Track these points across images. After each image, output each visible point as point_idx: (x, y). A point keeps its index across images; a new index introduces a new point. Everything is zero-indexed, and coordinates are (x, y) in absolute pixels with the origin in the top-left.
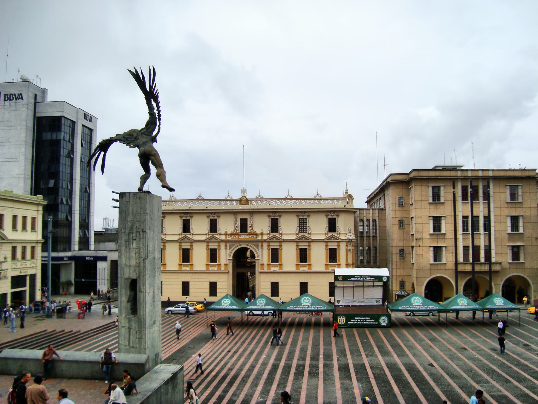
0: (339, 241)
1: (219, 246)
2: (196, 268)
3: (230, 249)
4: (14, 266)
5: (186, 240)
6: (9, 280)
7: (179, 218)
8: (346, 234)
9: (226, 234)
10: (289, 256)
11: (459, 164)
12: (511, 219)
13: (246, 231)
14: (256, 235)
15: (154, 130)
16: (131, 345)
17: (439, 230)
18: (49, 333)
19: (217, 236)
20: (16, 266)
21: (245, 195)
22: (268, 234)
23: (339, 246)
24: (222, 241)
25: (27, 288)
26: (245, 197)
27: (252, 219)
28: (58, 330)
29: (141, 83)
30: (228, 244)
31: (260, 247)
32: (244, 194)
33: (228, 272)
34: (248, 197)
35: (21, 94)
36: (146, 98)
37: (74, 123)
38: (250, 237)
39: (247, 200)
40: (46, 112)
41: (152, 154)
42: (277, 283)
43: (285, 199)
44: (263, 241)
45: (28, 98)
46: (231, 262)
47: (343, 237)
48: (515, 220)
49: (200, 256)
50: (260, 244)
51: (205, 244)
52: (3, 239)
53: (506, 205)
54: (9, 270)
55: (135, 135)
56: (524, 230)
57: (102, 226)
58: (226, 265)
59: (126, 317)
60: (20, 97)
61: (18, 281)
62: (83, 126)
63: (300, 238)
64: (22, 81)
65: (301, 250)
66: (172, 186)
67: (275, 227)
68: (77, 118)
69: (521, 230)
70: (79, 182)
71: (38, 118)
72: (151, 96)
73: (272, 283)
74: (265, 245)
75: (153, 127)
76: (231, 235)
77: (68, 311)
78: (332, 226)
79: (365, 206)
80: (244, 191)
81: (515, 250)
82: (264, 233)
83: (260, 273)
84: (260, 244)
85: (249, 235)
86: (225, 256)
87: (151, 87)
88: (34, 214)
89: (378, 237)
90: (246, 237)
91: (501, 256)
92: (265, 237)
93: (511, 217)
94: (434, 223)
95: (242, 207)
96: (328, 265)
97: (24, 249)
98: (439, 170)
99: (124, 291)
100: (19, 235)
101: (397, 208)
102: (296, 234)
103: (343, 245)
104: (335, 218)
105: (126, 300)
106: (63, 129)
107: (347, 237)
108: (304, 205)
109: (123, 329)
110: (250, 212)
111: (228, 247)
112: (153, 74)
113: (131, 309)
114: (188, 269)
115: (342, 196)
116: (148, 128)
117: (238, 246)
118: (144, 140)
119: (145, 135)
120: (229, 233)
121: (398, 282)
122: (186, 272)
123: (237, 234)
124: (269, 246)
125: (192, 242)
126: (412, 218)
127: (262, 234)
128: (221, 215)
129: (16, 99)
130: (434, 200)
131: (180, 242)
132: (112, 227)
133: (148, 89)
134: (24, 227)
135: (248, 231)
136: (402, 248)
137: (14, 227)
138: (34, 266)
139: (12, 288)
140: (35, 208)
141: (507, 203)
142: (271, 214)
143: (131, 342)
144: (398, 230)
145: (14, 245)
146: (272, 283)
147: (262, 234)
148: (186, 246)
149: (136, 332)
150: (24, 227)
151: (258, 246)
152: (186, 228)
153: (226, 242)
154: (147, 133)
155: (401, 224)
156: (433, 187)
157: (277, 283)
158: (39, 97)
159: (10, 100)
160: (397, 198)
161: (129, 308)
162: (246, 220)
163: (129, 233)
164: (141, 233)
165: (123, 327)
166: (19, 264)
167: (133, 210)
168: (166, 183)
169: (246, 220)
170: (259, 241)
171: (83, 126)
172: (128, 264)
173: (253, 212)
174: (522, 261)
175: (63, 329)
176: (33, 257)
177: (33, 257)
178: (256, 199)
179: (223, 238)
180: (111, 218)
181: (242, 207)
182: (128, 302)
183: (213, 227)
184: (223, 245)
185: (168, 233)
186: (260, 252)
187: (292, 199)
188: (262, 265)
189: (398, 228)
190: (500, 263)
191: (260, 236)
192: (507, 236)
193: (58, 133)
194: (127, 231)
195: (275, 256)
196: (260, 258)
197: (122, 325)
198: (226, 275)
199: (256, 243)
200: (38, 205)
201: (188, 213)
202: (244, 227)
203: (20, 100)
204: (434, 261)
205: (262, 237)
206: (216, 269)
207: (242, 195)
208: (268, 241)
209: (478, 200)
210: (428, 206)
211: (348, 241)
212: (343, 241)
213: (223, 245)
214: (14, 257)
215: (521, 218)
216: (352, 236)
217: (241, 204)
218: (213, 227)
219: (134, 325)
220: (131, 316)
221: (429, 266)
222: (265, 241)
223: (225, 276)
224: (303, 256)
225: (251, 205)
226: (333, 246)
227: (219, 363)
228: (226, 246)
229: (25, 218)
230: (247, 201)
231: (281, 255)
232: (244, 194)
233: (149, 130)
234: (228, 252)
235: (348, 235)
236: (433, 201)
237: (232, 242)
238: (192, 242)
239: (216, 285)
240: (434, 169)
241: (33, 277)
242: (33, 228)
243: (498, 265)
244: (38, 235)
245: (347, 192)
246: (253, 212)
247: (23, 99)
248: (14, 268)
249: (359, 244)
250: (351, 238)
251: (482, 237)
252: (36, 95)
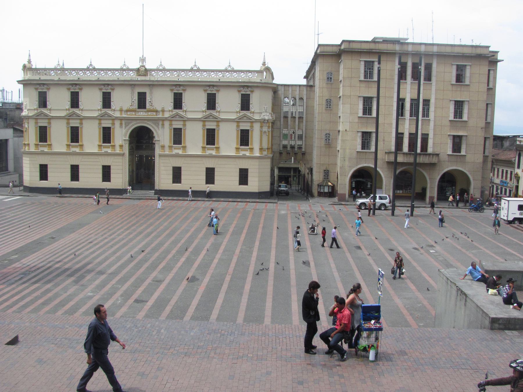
0: (252, 122)
1: (113, 124)
5: (211, 119)
7: (34, 90)
8: (261, 113)
9: (121, 110)
10: (194, 137)
11: (401, 36)
12: (455, 104)
13: (145, 107)
14: (157, 111)
17: (461, 117)
21: (145, 64)
22: (170, 111)
23: (252, 127)
24: (117, 118)
26: (144, 66)
27: (151, 93)
30: (123, 122)
31: (160, 126)
32: (143, 63)
33: (123, 155)
38: (149, 113)
39: (146, 70)
43: (191, 70)
44: (163, 120)
46: (127, 142)
47: (257, 117)
48: (459, 105)
50: (161, 123)
53: (450, 87)
56: (468, 118)
58: (121, 146)
63: (240, 118)
65: (242, 131)
67: (178, 103)
69: (465, 118)
74: (167, 124)
76: (127, 111)
77: (504, 310)
78: (245, 104)
79: (304, 82)
80: (143, 60)
81: (457, 140)
83: (160, 156)
84: (161, 123)
86: (121, 136)
89: (304, 119)
90: (144, 114)
91: (439, 144)
92: (167, 115)
93: (456, 101)
94: (364, 105)
95: (140, 78)
98: (378, 42)
101: (324, 84)
103: (257, 127)
107: (262, 117)
108: (214, 77)
110: (149, 85)
111: (124, 125)
115: (258, 69)
120: (125, 109)
121: (322, 171)
124: (171, 125)
126: (340, 97)
127: (163, 111)
128: (83, 87)
130: (365, 77)
131: (68, 118)
135: (147, 107)
136: (328, 132)
141: (452, 85)
144: (324, 111)
147: (163, 111)
151: (159, 125)
152: (75, 102)
153: (163, 120)
155: (329, 104)
156: (365, 61)
160: (325, 73)
162: (145, 94)
169: (145, 94)
170: (159, 119)
174: (463, 153)
178: (158, 70)
179: (117, 114)
181: (140, 78)
183: (107, 102)
184: (117, 123)
185: (222, 110)
186: (160, 131)
187: (199, 70)
189: (324, 108)
190: (438, 155)
191: (161, 113)
192: (448, 124)
195: (178, 137)
196: (160, 139)
198: (121, 157)
199: (156, 121)
204: (362, 149)
205: (163, 115)
206: (109, 151)
207: (141, 64)
208: (171, 120)
209: (405, 79)
210: (358, 84)
211: (263, 122)
212: (257, 121)
215: (466, 103)
216: (267, 116)
217: (140, 75)
218: (107, 102)
221: (355, 153)
222: (166, 119)
223: (119, 159)
225: (151, 77)
226: (245, 126)
228: (121, 124)
231: (185, 134)
232: (143, 63)
234: (124, 131)
235: (263, 114)
236: (365, 78)
240: (374, 41)
243: (434, 157)
245: (264, 64)
249: (282, 126)
250: (267, 118)
251: (407, 122)
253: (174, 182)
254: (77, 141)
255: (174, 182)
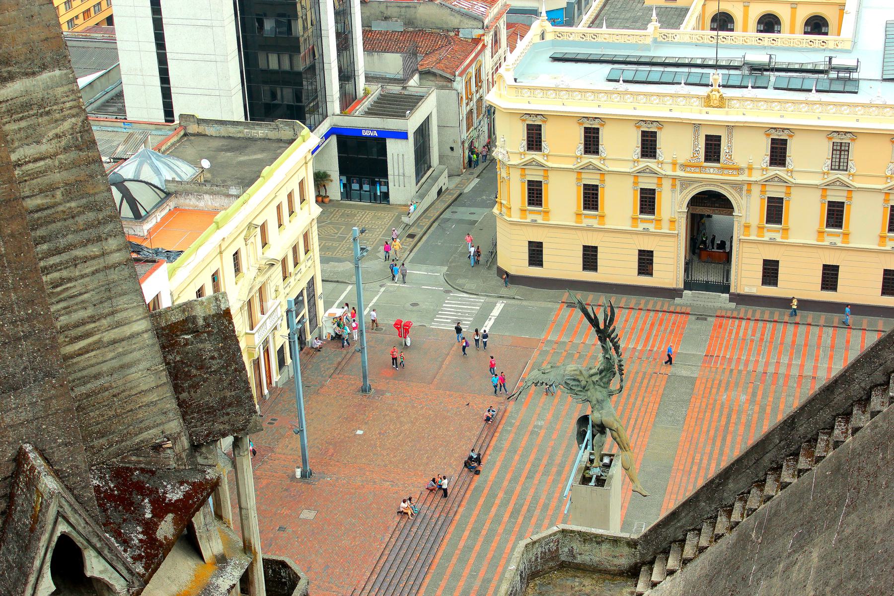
10: (562, 197)
14: (739, 170)
31: (744, 193)
49: (619, 201)
58: (672, 222)
65: (586, 187)
76: (684, 166)
84: (745, 187)
86: (673, 206)
92: (757, 176)
96: (823, 232)
104: (598, 129)
114: (594, 223)
120: (681, 161)
124: (763, 192)
127: (750, 169)
151: (741, 190)
170: (743, 182)
179: (668, 171)
186: (743, 202)
188: (747, 227)
191: (746, 171)
196: (743, 213)
199: (737, 186)
223: (671, 242)
231: (849, 215)
237: (686, 183)
253: (764, 283)
254: (779, 221)
255: (764, 283)
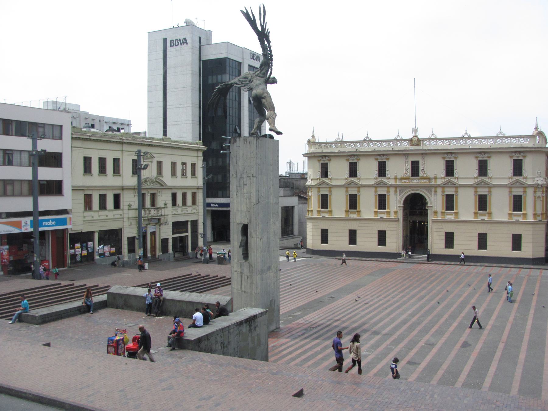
0: (525, 187)
1: (388, 191)
2: (364, 216)
3: (400, 194)
4: (174, 212)
6: (171, 224)
9: (396, 179)
13: (418, 175)
14: (429, 179)
15: (268, 72)
16: (243, 289)
18: (203, 277)
19: (487, 180)
20: (177, 212)
21: (417, 134)
22: (442, 178)
24: (391, 186)
25: (189, 234)
26: (416, 136)
27: (424, 161)
28: (202, 275)
29: (252, 23)
30: (398, 190)
31: (433, 193)
32: (415, 133)
33: (397, 220)
34: (420, 137)
35: (185, 39)
36: (259, 39)
37: (240, 64)
38: (422, 181)
39: (419, 140)
40: (210, 55)
41: (263, 96)
42: (326, 231)
43: (462, 138)
44: (436, 187)
45: (192, 42)
46: (402, 209)
47: (530, 182)
50: (433, 190)
51: (473, 190)
52: (162, 186)
54: (170, 216)
55: (249, 78)
57: (286, 171)
58: (396, 212)
59: (238, 261)
60: (184, 42)
61: (178, 226)
62: (249, 66)
64: (185, 24)
65: (380, 196)
66: (279, 130)
67: (450, 170)
68: (243, 58)
70: (248, 125)
71: (203, 61)
72: (263, 36)
73: (447, 234)
74: (439, 190)
75: (266, 68)
76: (401, 179)
78: (518, 169)
80: (415, 130)
82: (438, 177)
83: (433, 221)
84: (433, 190)
85: (421, 179)
86: (396, 203)
87: (262, 26)
88: (194, 160)
90: (418, 181)
92: (439, 182)
97: (184, 196)
99: (236, 236)
100: (179, 181)
102: (509, 178)
105: (239, 245)
106: (227, 72)
107: (535, 182)
108: (485, 144)
109: (236, 273)
110: (422, 154)
111: (398, 193)
112: (263, 12)
113: (243, 254)
114: (327, 216)
115: (530, 134)
116: (262, 70)
117: (409, 191)
118: (258, 82)
119: (259, 77)
120: (399, 177)
122: (324, 219)
123: (408, 179)
124: (443, 191)
125: (331, 187)
127: (436, 178)
129: (181, 44)
131: (347, 186)
132: (296, 172)
133: (260, 28)
134: (184, 174)
137: (174, 173)
138: (196, 212)
139: (173, 233)
140: (195, 154)
142: (479, 155)
143: (243, 287)
145: (174, 191)
146: (447, 234)
147: (436, 178)
148: (353, 191)
149: (248, 277)
150: (184, 174)
152: (353, 172)
154: (261, 75)
157: (326, 231)
158: (203, 39)
159: (176, 45)
161: (241, 253)
162: (418, 162)
163: (240, 178)
164: (251, 178)
165: (235, 271)
166: (180, 211)
167: (243, 154)
168: (274, 126)
169: (418, 162)
171: (249, 66)
172: (240, 209)
173: (426, 154)
175: (224, 275)
176: (194, 202)
177: (194, 202)
178: (430, 139)
179: (392, 182)
180: (295, 162)
181: (413, 148)
182: (240, 247)
183: (382, 171)
184: (392, 190)
185: (494, 176)
191: (433, 180)
193: (224, 76)
194: (239, 176)
195: (450, 203)
196: (433, 205)
197: (235, 269)
198: (396, 223)
199: (428, 188)
200: (198, 150)
201: (354, 155)
202: (415, 170)
203: (185, 44)
205: (436, 182)
207: (414, 134)
208: (443, 186)
211: (536, 187)
212: (530, 186)
213: (392, 190)
214: (174, 203)
217: (413, 145)
218: (382, 171)
219: (246, 270)
220: (243, 261)
222: (439, 186)
223: (393, 225)
224: (353, 202)
225: (424, 146)
227: (351, 313)
228: (396, 191)
229: (184, 164)
230: (419, 141)
231: (331, 202)
232: (415, 133)
233: (262, 72)
234: (398, 198)
235: (537, 179)
238: (389, 187)
239: (356, 233)
241: (195, 223)
242: (194, 174)
244: (199, 180)
245: (536, 128)
246: (426, 154)
247: (187, 43)
248: (175, 214)
250: (540, 183)
252: (200, 38)
